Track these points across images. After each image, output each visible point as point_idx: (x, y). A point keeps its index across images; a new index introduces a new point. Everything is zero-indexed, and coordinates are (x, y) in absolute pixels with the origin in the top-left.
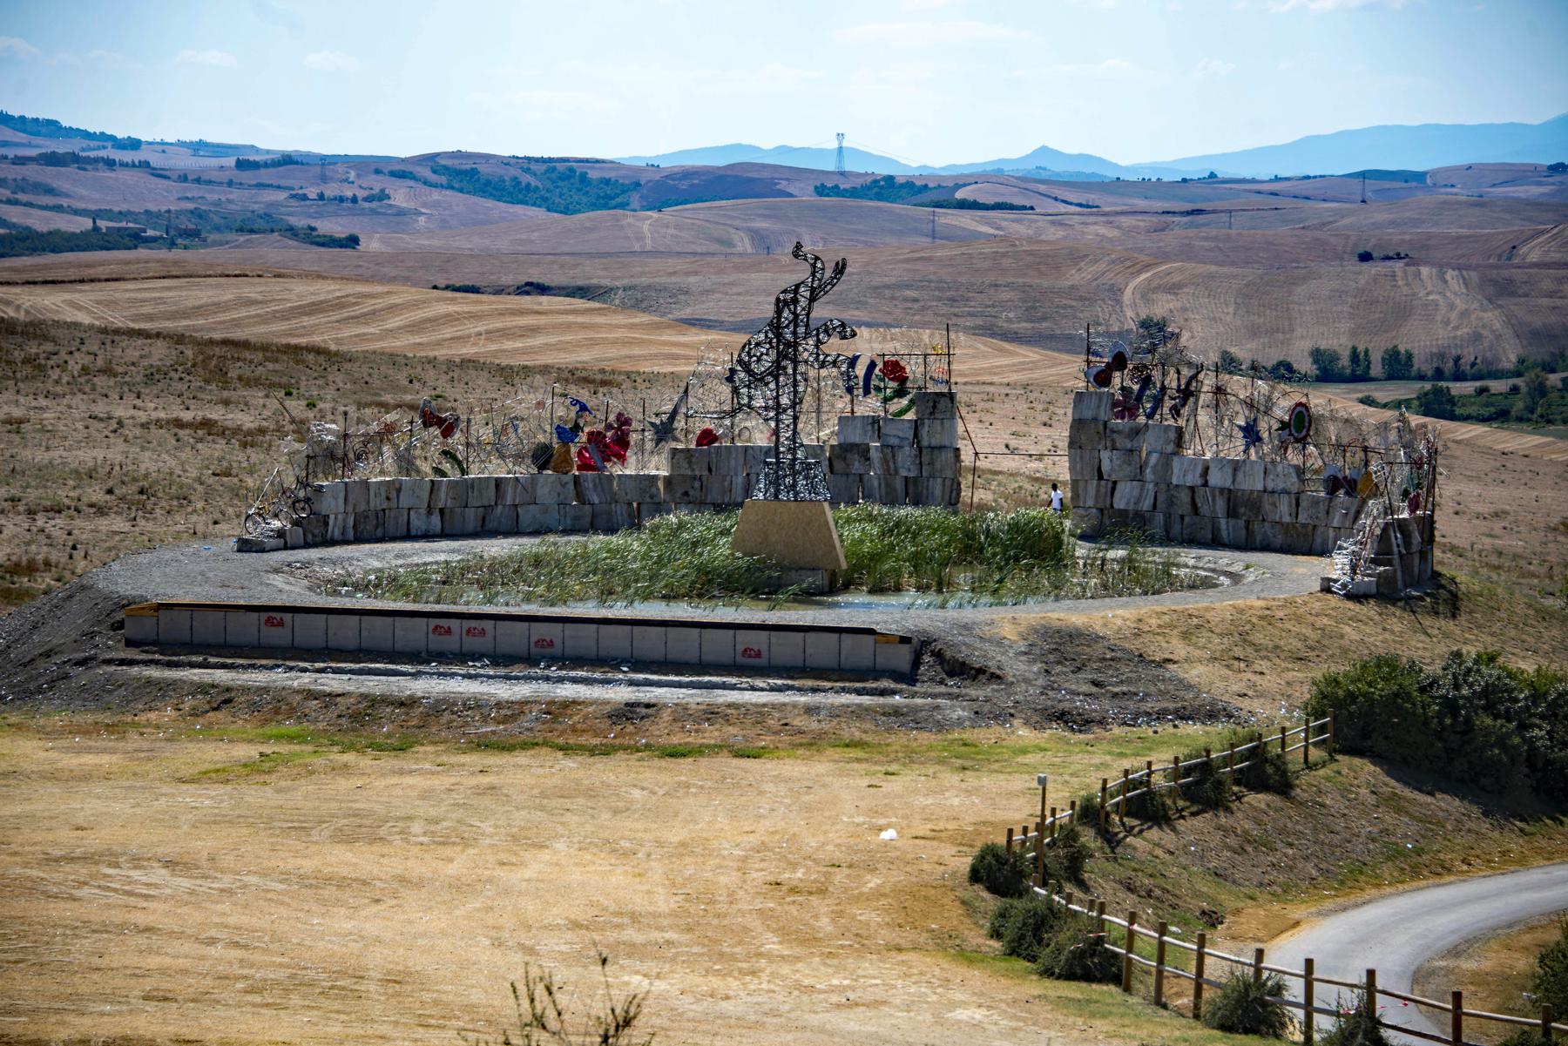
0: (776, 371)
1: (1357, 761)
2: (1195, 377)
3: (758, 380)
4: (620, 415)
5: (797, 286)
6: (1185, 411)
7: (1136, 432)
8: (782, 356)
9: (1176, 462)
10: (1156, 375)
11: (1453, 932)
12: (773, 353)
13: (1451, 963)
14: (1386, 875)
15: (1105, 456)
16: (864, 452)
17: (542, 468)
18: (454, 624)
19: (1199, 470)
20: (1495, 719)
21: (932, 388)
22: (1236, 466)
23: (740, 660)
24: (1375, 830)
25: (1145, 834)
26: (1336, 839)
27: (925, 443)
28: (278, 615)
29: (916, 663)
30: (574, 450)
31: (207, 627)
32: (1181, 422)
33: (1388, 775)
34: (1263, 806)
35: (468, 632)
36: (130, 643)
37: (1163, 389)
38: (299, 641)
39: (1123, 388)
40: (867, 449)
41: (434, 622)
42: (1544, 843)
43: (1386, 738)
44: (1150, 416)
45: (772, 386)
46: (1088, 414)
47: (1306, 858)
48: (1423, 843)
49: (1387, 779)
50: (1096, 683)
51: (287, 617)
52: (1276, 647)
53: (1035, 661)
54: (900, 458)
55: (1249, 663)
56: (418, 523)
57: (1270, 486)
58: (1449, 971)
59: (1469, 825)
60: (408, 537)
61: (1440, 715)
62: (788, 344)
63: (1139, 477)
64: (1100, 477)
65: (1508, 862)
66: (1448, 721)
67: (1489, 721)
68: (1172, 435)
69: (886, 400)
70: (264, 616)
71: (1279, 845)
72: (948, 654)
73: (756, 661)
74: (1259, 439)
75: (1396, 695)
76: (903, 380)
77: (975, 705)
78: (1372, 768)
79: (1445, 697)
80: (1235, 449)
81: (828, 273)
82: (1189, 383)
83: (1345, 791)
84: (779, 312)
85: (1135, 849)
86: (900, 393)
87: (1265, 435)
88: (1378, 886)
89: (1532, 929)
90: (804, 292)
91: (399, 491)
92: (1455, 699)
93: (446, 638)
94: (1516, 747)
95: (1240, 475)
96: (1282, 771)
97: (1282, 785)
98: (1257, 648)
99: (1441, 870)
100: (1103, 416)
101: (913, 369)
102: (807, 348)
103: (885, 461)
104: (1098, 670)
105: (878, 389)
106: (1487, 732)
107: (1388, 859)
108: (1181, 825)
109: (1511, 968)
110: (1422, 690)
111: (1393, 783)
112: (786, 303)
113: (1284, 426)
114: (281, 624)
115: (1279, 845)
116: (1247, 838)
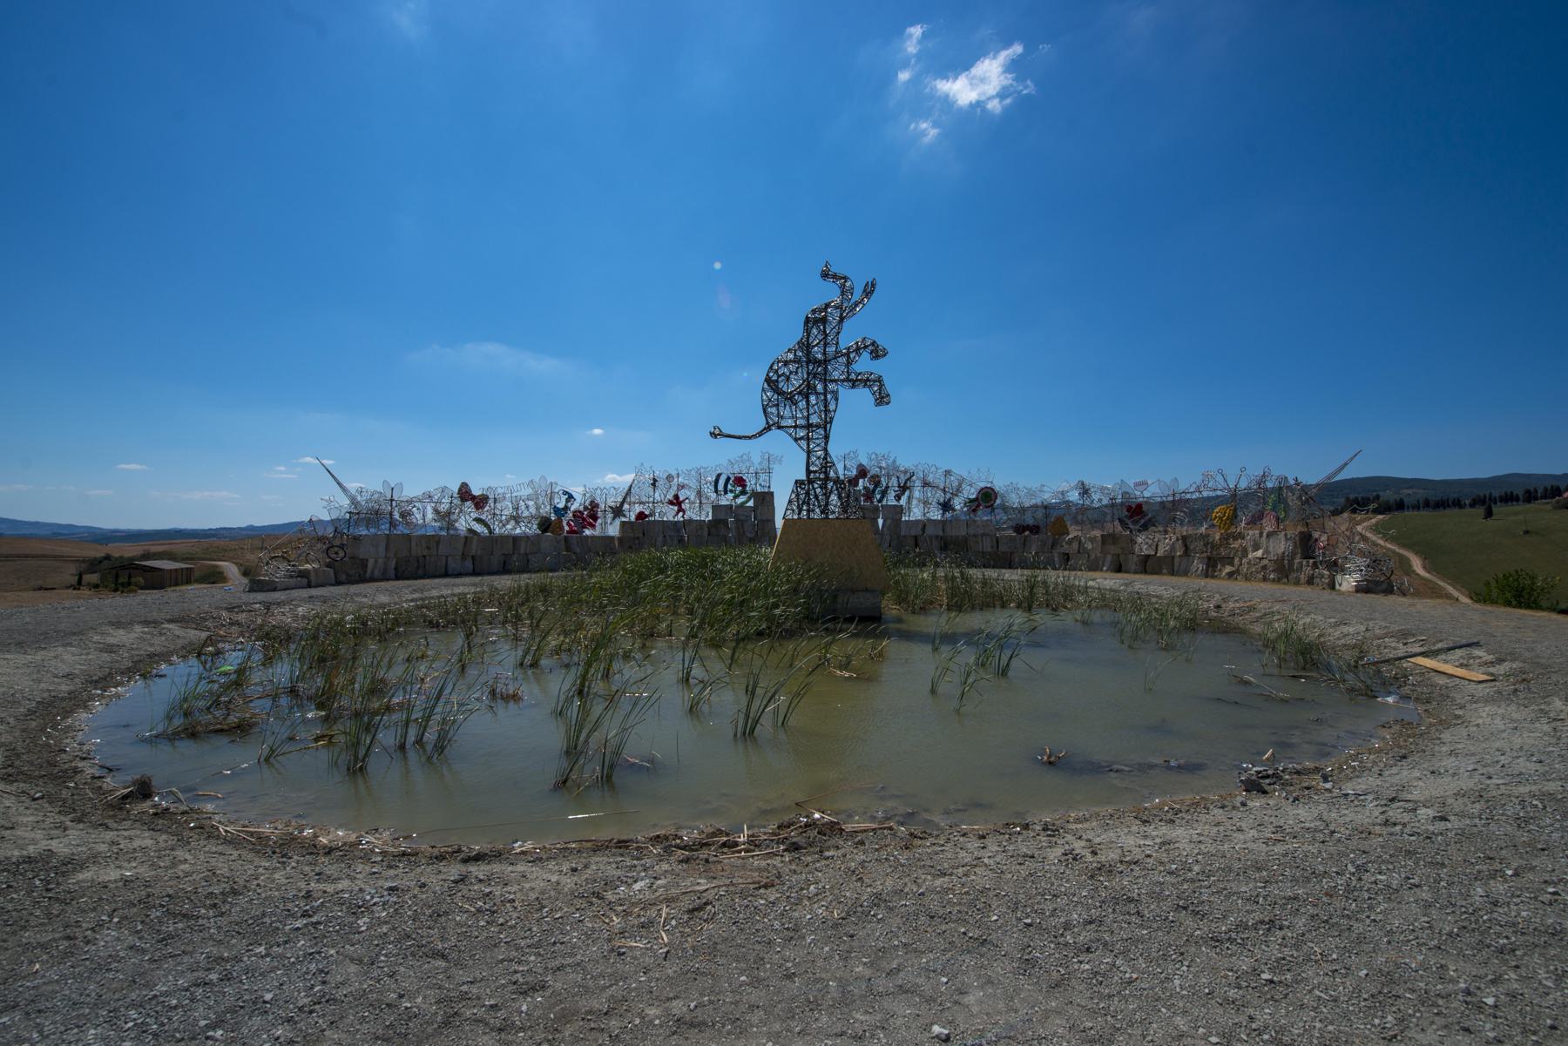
10: (884, 481)
12: (803, 373)
16: (725, 522)
17: (544, 531)
21: (759, 489)
56: (453, 565)
60: (446, 575)
62: (818, 362)
69: (736, 497)
76: (744, 486)
80: (936, 514)
84: (808, 332)
86: (743, 492)
91: (438, 543)
112: (816, 321)
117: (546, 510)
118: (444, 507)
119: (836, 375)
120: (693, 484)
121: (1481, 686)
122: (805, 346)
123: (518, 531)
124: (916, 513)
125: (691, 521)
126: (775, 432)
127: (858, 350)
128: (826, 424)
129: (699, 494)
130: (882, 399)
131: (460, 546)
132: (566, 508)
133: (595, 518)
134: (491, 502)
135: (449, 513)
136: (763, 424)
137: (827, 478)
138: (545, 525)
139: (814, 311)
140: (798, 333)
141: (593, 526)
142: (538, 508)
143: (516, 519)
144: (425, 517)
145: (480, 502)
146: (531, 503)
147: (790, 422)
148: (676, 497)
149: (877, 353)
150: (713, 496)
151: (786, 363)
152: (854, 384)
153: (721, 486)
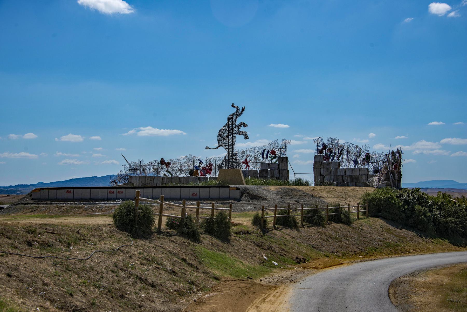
0: (228, 136)
1: (376, 219)
2: (342, 150)
3: (224, 138)
4: (209, 163)
5: (233, 114)
6: (340, 158)
7: (329, 164)
8: (229, 132)
9: (338, 170)
10: (333, 150)
11: (411, 268)
13: (411, 279)
14: (385, 252)
15: (322, 170)
16: (267, 171)
18: (114, 190)
19: (344, 171)
20: (422, 207)
21: (282, 156)
22: (352, 170)
23: (191, 197)
24: (381, 238)
25: (283, 230)
26: (366, 240)
27: (280, 169)
28: (70, 190)
29: (242, 196)
30: (199, 172)
31: (53, 194)
32: (340, 161)
33: (387, 223)
34: (339, 227)
35: (118, 192)
36: (33, 199)
37: (335, 153)
38: (75, 197)
39: (326, 154)
40: (267, 171)
41: (109, 190)
42: (441, 247)
43: (386, 212)
44: (332, 160)
45: (227, 140)
46: (318, 160)
47: (354, 245)
48: (399, 243)
49: (386, 224)
50: (296, 201)
51: (72, 190)
52: (355, 196)
53: (278, 195)
54: (275, 172)
55: (346, 199)
57: (361, 173)
58: (410, 282)
59: (415, 239)
61: (404, 206)
62: (231, 129)
63: (330, 174)
64: (321, 175)
65: (429, 251)
66: (406, 207)
67: (420, 207)
68: (337, 164)
69: (272, 160)
70: (66, 190)
71: (343, 240)
72: (251, 193)
73: (196, 197)
74: (358, 163)
75: (389, 198)
77: (255, 206)
78: (381, 221)
79: (405, 200)
80: (352, 166)
81: (241, 110)
82: (341, 151)
83: (371, 226)
84: (228, 121)
85: (275, 234)
86: (275, 158)
87: (359, 162)
88: (381, 255)
89: (445, 268)
90: (235, 116)
92: (409, 200)
93: (112, 194)
94: (429, 216)
95: (353, 172)
96: (348, 217)
97: (348, 222)
98: (349, 196)
99: (406, 252)
100: (321, 160)
101: (277, 152)
102: (235, 131)
103: (271, 173)
104: (298, 198)
105: (270, 157)
106: (420, 211)
107: (386, 247)
108: (302, 230)
109: (442, 281)
110: (397, 197)
111: (388, 225)
113: (364, 159)
114: (71, 192)
115: (343, 240)
116: (330, 236)
117: (192, 167)
118: (156, 167)
119: (235, 132)
120: (253, 154)
121: (202, 189)
122: (228, 125)
123: (181, 176)
124: (344, 166)
125: (252, 170)
126: (221, 147)
127: (240, 125)
128: (233, 144)
129: (256, 158)
130: (246, 138)
131: (161, 180)
132: (199, 166)
133: (211, 170)
134: (172, 164)
135: (158, 169)
136: (217, 145)
137: (233, 159)
138: (191, 172)
139: (230, 116)
140: (226, 122)
141: (210, 173)
142: (189, 166)
143: (180, 170)
144: (150, 171)
145: (168, 165)
146: (186, 165)
147: (224, 145)
148: (246, 160)
149: (245, 125)
150: (262, 159)
151: (223, 130)
152: (240, 134)
153: (265, 155)
